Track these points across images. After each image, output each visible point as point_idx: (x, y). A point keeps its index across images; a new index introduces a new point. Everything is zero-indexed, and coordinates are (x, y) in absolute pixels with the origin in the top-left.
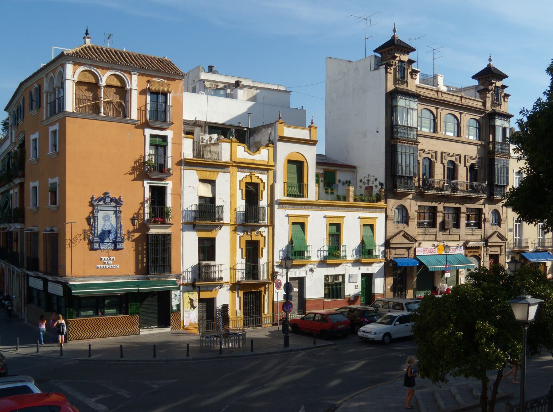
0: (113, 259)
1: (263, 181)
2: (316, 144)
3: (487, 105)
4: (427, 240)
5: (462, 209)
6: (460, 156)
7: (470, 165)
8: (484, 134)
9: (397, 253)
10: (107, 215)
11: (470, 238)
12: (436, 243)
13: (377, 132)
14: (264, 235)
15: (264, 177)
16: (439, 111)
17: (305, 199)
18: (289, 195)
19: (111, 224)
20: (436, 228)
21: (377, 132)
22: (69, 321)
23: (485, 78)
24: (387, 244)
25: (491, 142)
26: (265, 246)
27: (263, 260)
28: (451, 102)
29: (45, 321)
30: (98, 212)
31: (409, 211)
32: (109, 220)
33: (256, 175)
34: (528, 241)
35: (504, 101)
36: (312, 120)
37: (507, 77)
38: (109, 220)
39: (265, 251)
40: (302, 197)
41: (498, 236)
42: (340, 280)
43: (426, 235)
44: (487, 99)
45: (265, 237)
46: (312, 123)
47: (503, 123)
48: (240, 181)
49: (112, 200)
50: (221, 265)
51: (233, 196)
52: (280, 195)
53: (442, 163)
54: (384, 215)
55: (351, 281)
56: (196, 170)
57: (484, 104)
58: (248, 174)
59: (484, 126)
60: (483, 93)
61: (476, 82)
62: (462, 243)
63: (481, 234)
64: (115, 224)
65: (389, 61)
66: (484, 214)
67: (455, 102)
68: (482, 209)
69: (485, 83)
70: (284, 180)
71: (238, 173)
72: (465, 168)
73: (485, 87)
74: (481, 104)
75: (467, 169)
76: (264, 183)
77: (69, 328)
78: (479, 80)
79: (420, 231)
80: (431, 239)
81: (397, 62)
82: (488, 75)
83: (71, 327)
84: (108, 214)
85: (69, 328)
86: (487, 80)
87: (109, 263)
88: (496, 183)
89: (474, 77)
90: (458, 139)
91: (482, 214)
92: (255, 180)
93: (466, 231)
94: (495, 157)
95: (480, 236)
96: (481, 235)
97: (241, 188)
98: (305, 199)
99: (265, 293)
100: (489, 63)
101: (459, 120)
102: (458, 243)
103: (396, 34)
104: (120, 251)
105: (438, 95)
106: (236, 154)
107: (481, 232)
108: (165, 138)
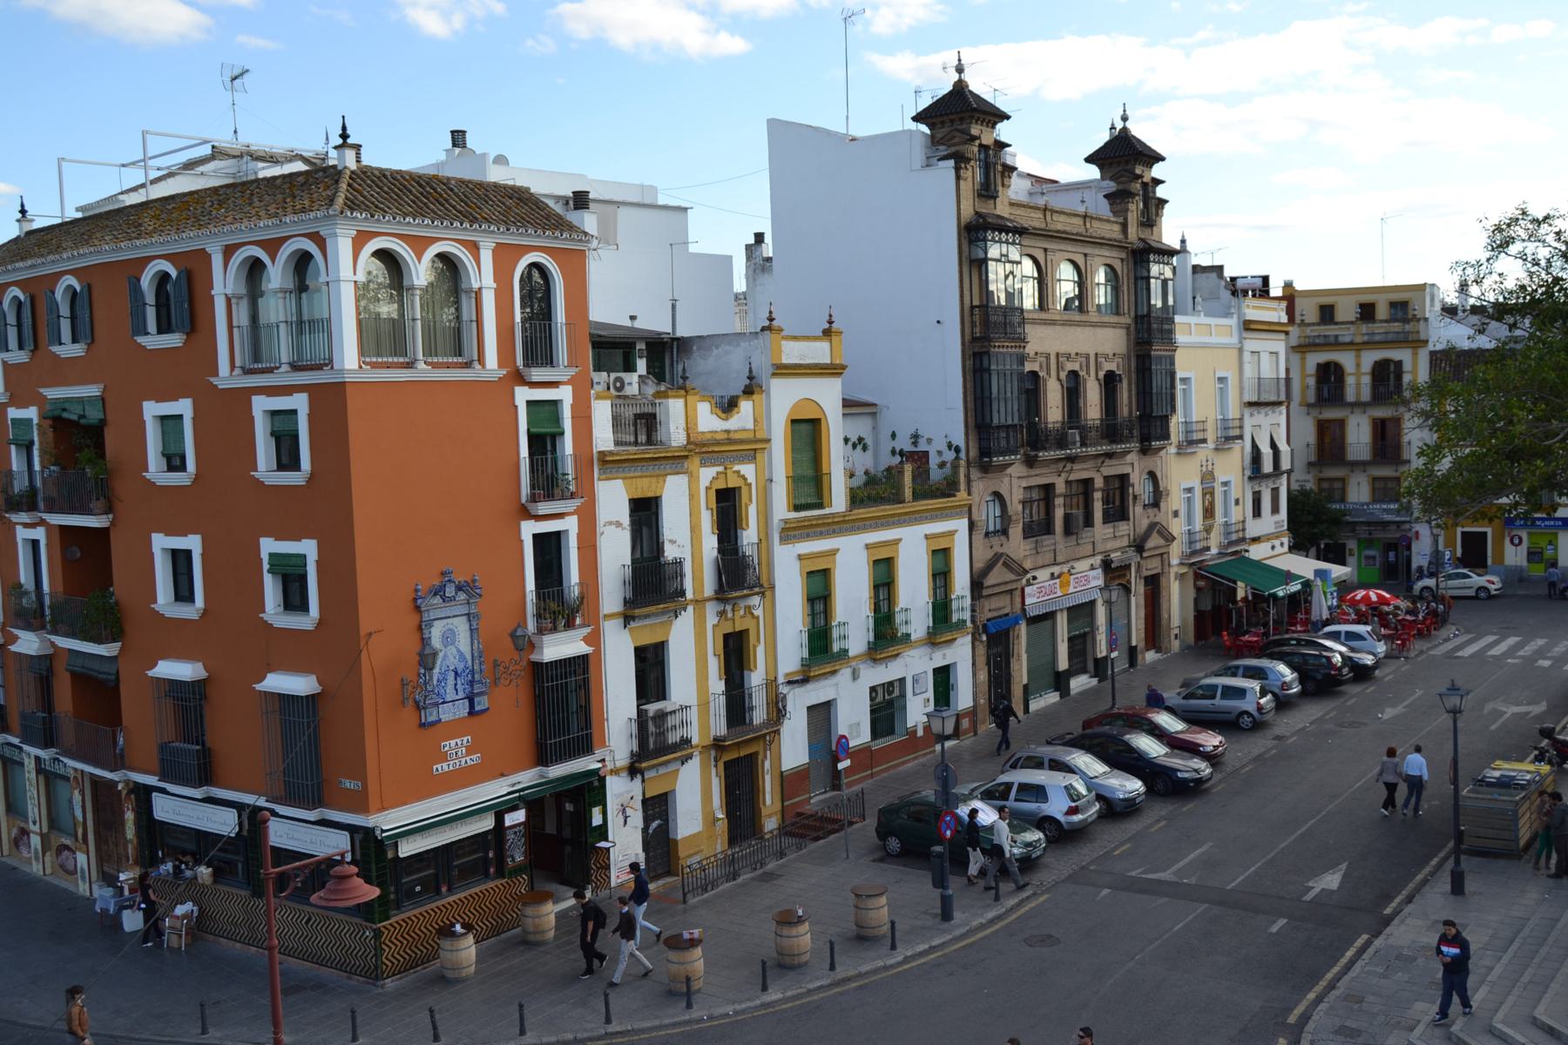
0: (468, 741)
1: (749, 481)
2: (841, 374)
3: (1129, 231)
4: (1041, 564)
5: (1057, 486)
6: (1048, 356)
7: (1105, 376)
8: (1126, 298)
9: (993, 607)
10: (449, 630)
11: (1110, 546)
12: (1056, 570)
13: (938, 322)
14: (756, 613)
15: (748, 470)
16: (1049, 258)
17: (827, 511)
18: (797, 508)
19: (459, 651)
20: (1054, 534)
21: (938, 322)
22: (382, 929)
23: (952, 121)
24: (977, 585)
25: (977, 307)
26: (759, 641)
27: (756, 678)
28: (1073, 234)
29: (41, 390)
30: (431, 626)
31: (1008, 503)
32: (453, 644)
33: (736, 468)
34: (906, 616)
35: (1003, 185)
36: (830, 316)
37: (1163, 159)
38: (453, 644)
39: (760, 652)
40: (820, 506)
41: (1005, 564)
42: (896, 693)
43: (1038, 553)
44: (1130, 214)
45: (758, 618)
46: (771, 319)
47: (1004, 251)
48: (707, 488)
49: (459, 588)
50: (686, 707)
51: (695, 529)
52: (781, 510)
53: (1059, 379)
54: (965, 521)
55: (917, 691)
56: (623, 479)
57: (1124, 226)
58: (721, 469)
59: (1125, 279)
60: (1118, 201)
61: (1093, 172)
62: (1097, 560)
63: (1127, 532)
64: (469, 648)
65: (1126, 186)
66: (1133, 485)
67: (1068, 229)
68: (1128, 475)
69: (1122, 176)
70: (787, 472)
71: (702, 470)
72: (1096, 383)
73: (1121, 187)
74: (1117, 228)
75: (1100, 384)
76: (750, 485)
77: (383, 946)
78: (1101, 167)
79: (1028, 547)
80: (1047, 562)
81: (976, 149)
82: (951, 117)
83: (387, 942)
84: (451, 627)
85: (383, 946)
86: (957, 130)
87: (459, 753)
88: (995, 421)
89: (1089, 160)
90: (1043, 316)
91: (1129, 485)
92: (733, 483)
93: (1105, 532)
94: (992, 350)
95: (1126, 538)
96: (1129, 535)
97: (710, 506)
98: (827, 511)
99: (765, 757)
100: (956, 77)
101: (1083, 271)
102: (1091, 561)
103: (1129, 124)
104: (1459, 759)
105: (1085, 223)
106: (696, 424)
107: (1127, 527)
108: (555, 404)
